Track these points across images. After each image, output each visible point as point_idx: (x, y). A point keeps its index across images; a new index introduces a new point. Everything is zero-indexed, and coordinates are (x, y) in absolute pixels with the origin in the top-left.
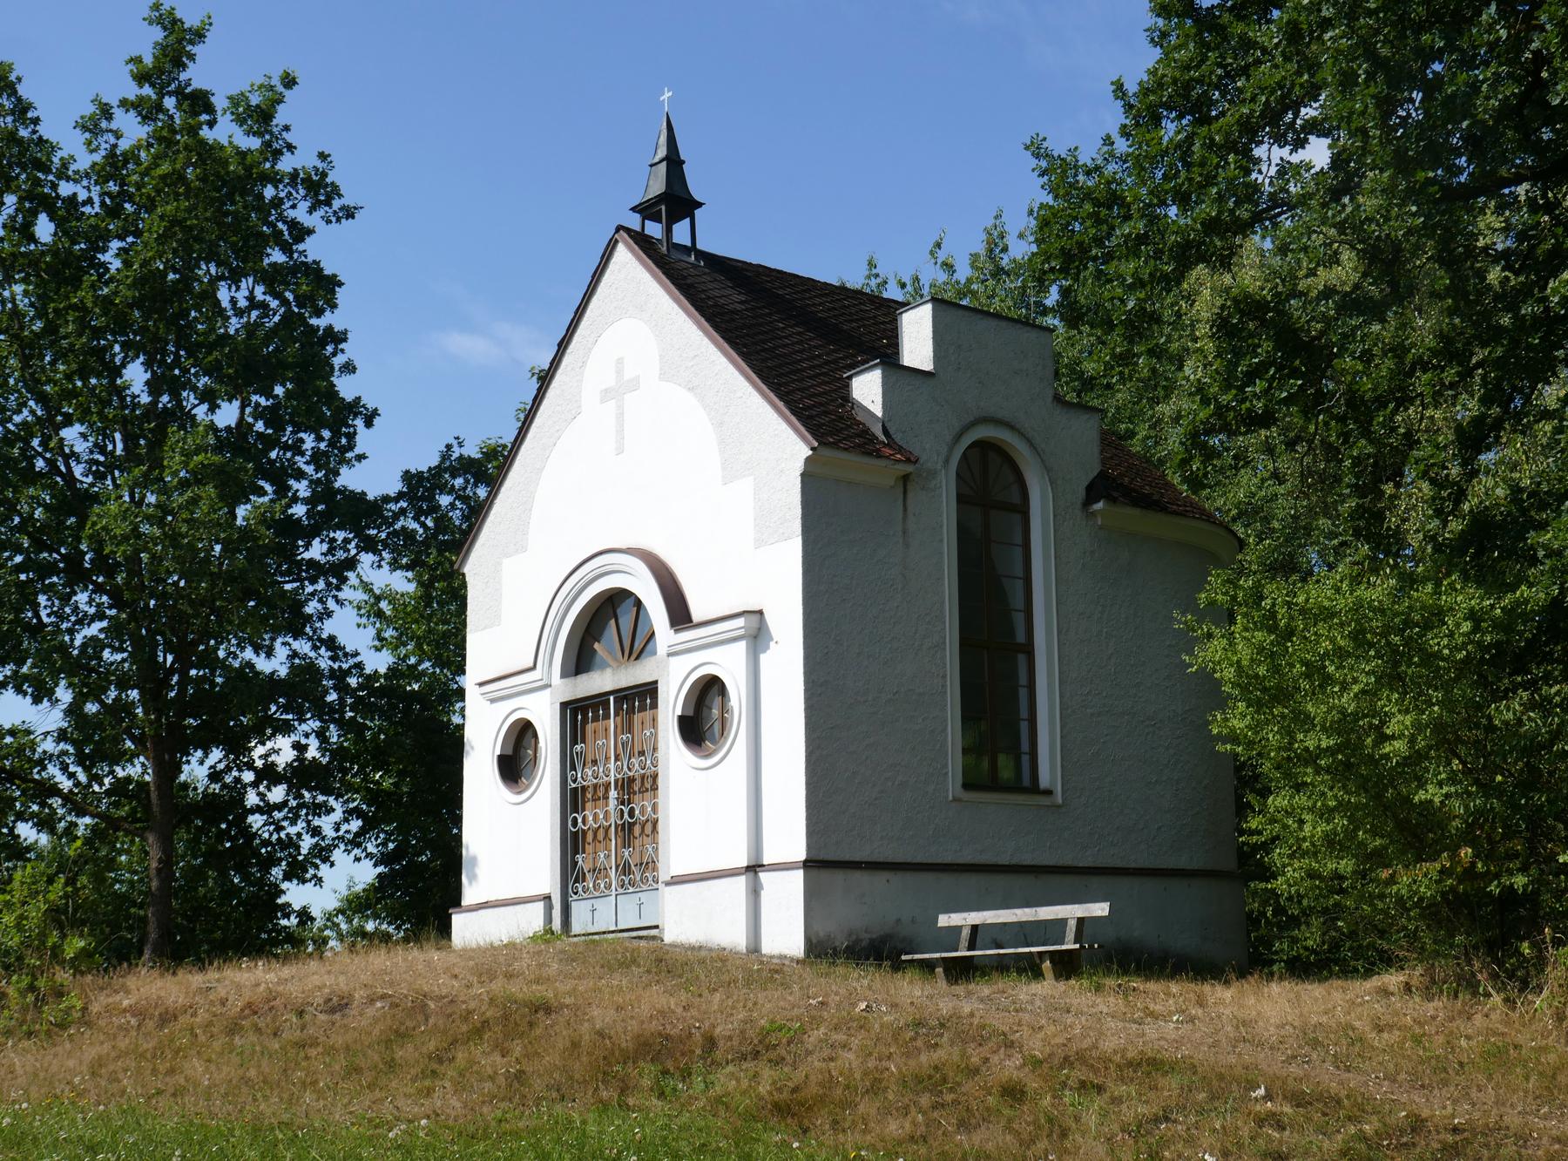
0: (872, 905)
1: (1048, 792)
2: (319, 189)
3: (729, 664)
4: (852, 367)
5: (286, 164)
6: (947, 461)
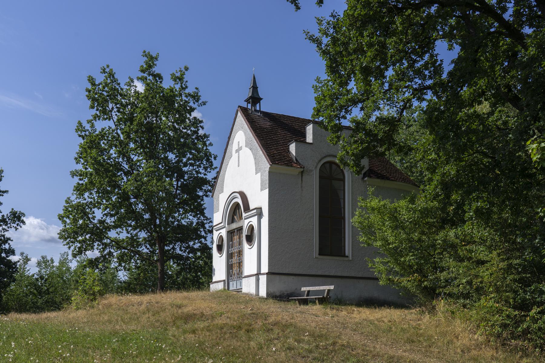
0: (284, 285)
1: (347, 257)
2: (196, 97)
3: (254, 221)
4: (290, 141)
5: (187, 91)
6: (316, 167)
